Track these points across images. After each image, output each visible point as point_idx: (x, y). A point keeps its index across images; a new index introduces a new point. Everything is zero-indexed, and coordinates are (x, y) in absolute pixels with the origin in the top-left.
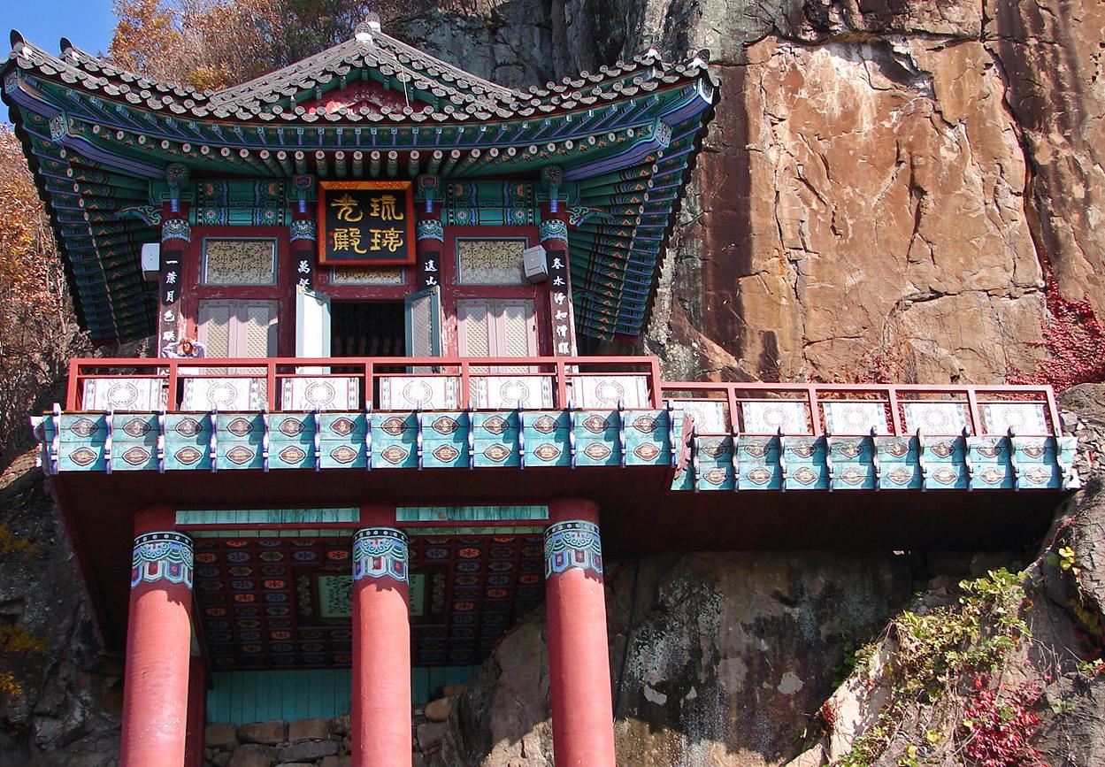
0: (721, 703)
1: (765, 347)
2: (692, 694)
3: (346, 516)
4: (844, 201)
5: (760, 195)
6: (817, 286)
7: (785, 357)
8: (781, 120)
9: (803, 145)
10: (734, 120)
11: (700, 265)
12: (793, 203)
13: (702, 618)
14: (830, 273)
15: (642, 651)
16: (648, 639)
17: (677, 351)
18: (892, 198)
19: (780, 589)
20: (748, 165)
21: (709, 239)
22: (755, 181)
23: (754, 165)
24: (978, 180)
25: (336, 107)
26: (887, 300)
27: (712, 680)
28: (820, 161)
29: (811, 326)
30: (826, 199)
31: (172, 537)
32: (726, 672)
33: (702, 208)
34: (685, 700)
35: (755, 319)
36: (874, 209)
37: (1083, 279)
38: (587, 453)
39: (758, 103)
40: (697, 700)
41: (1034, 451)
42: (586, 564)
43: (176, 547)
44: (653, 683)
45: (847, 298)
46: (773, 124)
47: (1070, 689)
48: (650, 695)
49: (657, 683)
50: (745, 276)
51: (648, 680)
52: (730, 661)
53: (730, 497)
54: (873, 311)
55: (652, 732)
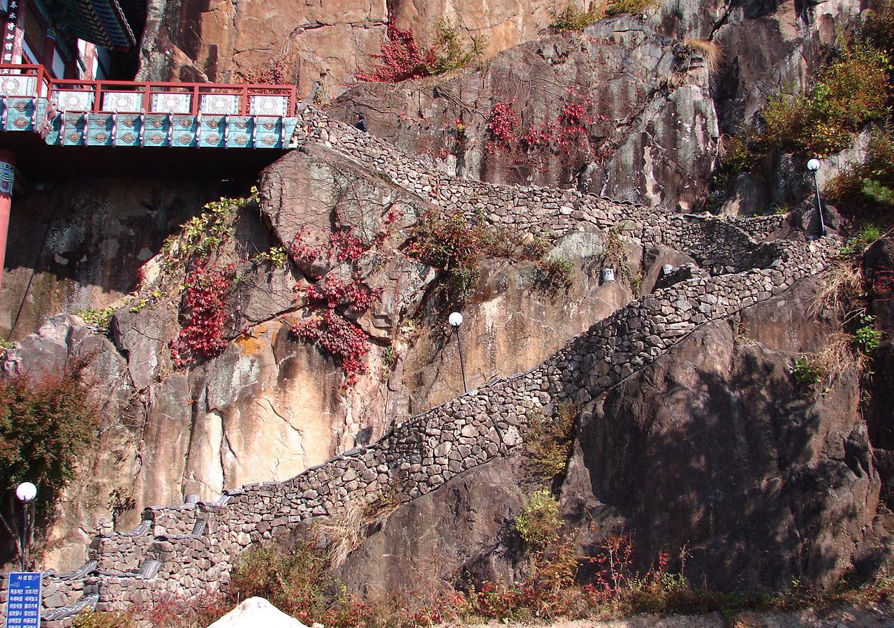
0: (101, 264)
2: (84, 259)
6: (247, 18)
7: (221, 60)
13: (96, 216)
14: (257, 11)
17: (157, 56)
26: (289, 27)
27: (98, 251)
29: (240, 42)
32: (106, 247)
35: (207, 38)
41: (269, 126)
45: (264, 26)
47: (250, 268)
48: (58, 259)
52: (110, 241)
53: (58, 147)
54: (279, 34)
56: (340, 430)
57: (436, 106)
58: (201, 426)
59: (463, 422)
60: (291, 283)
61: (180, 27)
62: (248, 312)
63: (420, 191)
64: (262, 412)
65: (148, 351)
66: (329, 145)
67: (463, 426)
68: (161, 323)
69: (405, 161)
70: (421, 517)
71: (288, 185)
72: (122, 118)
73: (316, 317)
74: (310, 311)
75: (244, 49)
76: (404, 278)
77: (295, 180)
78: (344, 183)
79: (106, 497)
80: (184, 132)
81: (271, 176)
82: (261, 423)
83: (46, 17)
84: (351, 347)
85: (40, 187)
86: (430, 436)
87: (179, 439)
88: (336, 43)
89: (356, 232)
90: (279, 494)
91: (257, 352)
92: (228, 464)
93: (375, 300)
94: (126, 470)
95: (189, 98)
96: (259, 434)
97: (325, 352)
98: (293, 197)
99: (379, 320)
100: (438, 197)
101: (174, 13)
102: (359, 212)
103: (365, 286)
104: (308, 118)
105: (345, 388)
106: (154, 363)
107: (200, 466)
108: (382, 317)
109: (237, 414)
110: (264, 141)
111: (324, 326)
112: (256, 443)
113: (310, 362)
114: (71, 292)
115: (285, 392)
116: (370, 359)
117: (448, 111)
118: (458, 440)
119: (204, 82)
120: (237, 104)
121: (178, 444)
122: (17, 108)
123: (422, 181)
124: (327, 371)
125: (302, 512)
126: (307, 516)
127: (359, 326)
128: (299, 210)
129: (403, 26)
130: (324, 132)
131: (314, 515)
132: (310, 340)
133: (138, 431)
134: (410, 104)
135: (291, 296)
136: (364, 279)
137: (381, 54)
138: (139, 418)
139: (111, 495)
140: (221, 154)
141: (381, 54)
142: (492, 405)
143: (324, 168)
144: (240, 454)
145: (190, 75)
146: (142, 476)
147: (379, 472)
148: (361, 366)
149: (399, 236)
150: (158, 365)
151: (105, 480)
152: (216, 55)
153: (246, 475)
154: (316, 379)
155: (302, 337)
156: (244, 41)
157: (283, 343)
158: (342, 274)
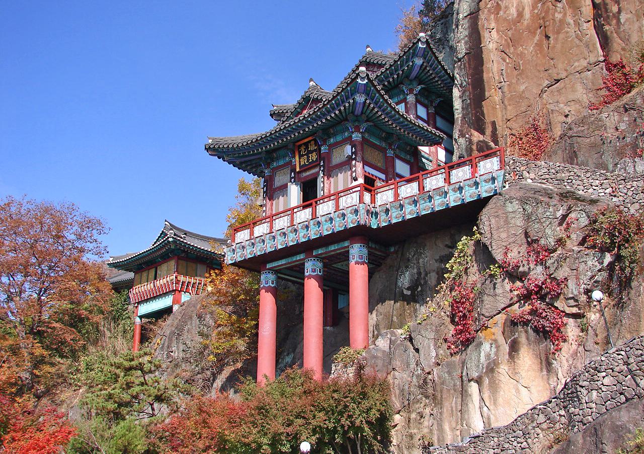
2: (419, 289)
3: (302, 256)
5: (487, 65)
8: (493, 29)
9: (502, 36)
10: (475, 37)
12: (499, 63)
13: (421, 260)
17: (462, 141)
18: (539, 45)
19: (447, 243)
21: (471, 90)
22: (485, 60)
23: (484, 53)
24: (572, 22)
25: (305, 112)
26: (536, 91)
27: (426, 282)
28: (509, 40)
30: (511, 56)
31: (266, 272)
32: (430, 279)
33: (468, 78)
34: (417, 292)
35: (488, 119)
37: (620, 50)
38: (339, 226)
39: (483, 26)
40: (421, 291)
41: (488, 180)
45: (521, 96)
46: (490, 32)
48: (405, 292)
52: (431, 274)
53: (379, 228)
54: (531, 98)
55: (407, 305)
56: (555, 384)
57: (627, 119)
58: (466, 391)
59: (604, 374)
60: (508, 285)
61: (472, 116)
62: (484, 311)
63: (603, 194)
64: (502, 378)
65: (429, 347)
66: (529, 181)
67: (604, 377)
68: (434, 328)
69: (588, 175)
70: (573, 450)
71: (493, 221)
72: (407, 201)
73: (527, 308)
74: (524, 303)
75: (512, 117)
76: (582, 267)
78: (529, 209)
79: (417, 442)
81: (482, 217)
82: (502, 385)
83: (384, 145)
84: (553, 324)
85: (392, 250)
86: (582, 387)
87: (454, 401)
88: (570, 90)
90: (502, 434)
91: (493, 337)
92: (485, 415)
93: (564, 287)
94: (426, 423)
95: (417, 184)
96: (502, 393)
97: (536, 330)
98: (498, 228)
99: (569, 301)
100: (618, 195)
101: (467, 109)
103: (555, 278)
104: (512, 167)
105: (554, 354)
106: (434, 354)
107: (469, 418)
108: (571, 298)
109: (486, 381)
110: (486, 191)
111: (534, 312)
112: (500, 399)
113: (528, 339)
114: (415, 310)
115: (514, 362)
116: (569, 330)
117: (638, 120)
118: (601, 389)
119: (492, 149)
120: (479, 168)
121: (453, 405)
122: (351, 213)
123: (604, 186)
124: (540, 343)
125: (515, 447)
126: (518, 450)
127: (557, 308)
128: (504, 235)
129: (615, 58)
130: (525, 173)
131: (523, 449)
132: (526, 323)
133: (430, 398)
134: (608, 124)
135: (509, 295)
137: (604, 86)
138: (429, 390)
139: (419, 440)
140: (448, 212)
141: (604, 86)
142: (628, 358)
143: (515, 203)
144: (491, 408)
145: (483, 146)
146: (435, 427)
147: (560, 416)
148: (562, 337)
149: (576, 237)
150: (437, 355)
151: (415, 431)
153: (497, 421)
154: (534, 350)
155: (520, 322)
156: (511, 112)
157: (509, 329)
158: (538, 274)
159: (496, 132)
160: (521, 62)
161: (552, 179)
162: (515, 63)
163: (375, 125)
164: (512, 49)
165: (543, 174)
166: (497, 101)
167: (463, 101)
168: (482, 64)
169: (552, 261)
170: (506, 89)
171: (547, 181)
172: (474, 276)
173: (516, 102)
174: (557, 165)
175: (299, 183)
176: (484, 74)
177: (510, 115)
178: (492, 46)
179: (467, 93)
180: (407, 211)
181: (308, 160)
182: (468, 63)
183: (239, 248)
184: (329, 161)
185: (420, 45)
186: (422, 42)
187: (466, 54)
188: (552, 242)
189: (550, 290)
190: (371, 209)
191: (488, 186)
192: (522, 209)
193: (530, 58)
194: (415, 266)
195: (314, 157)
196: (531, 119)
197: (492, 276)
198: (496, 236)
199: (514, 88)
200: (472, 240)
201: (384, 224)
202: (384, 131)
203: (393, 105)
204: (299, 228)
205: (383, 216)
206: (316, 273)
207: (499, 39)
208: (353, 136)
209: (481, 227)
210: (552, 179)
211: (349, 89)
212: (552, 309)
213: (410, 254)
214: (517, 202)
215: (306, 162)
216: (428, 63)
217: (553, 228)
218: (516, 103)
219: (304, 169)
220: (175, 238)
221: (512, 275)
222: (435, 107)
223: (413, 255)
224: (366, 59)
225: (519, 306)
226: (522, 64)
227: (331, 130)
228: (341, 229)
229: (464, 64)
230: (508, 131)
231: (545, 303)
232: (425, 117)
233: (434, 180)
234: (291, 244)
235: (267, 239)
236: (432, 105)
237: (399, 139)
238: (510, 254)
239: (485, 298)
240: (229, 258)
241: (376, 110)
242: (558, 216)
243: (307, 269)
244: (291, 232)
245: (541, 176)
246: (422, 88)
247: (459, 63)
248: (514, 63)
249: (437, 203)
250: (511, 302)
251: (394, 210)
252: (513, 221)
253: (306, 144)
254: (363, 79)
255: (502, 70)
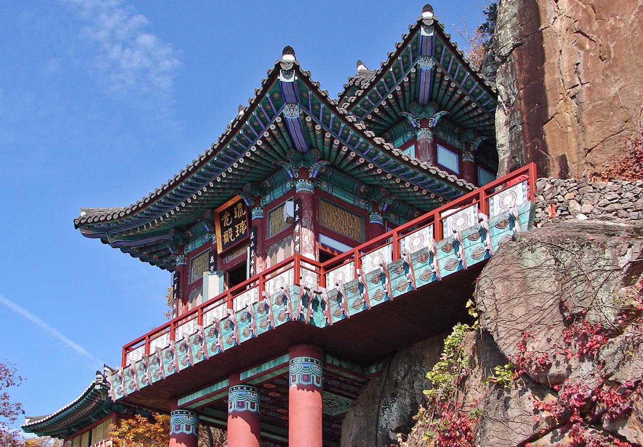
1: (561, 167)
3: (225, 384)
4: (608, 31)
5: (551, 60)
9: (577, 5)
11: (521, 129)
12: (571, 53)
15: (385, 412)
16: (388, 404)
20: (541, 43)
21: (523, 108)
22: (547, 51)
23: (545, 40)
30: (595, 37)
31: (176, 413)
35: (554, 153)
36: (631, 25)
38: (261, 327)
41: (502, 224)
42: (297, 382)
43: (178, 417)
44: (393, 429)
45: (612, 105)
49: (395, 429)
50: (546, 123)
51: (390, 428)
53: (328, 327)
54: (631, 106)
60: (529, 401)
61: (526, 152)
66: (581, 217)
71: (499, 287)
74: (563, 433)
75: (595, 144)
77: (507, 278)
80: (423, 269)
83: (362, 204)
85: (374, 371)
89: (592, 317)
98: (509, 300)
101: (517, 141)
102: (590, 289)
103: (617, 383)
104: (549, 196)
127: (623, 439)
128: (519, 311)
135: (532, 420)
136: (612, 374)
143: (539, 250)
152: (566, 164)
156: (594, 133)
158: (583, 377)
159: (567, 173)
160: (612, 45)
161: (625, 209)
162: (601, 49)
163: (333, 166)
164: (596, 25)
165: (608, 202)
166: (569, 120)
167: (511, 129)
168: (543, 60)
169: (611, 350)
170: (583, 97)
171: (616, 215)
172: (477, 391)
173: (603, 117)
174: (637, 185)
175: (222, 272)
176: (546, 76)
177: (592, 141)
178: (559, 25)
179: (518, 115)
180: (371, 294)
181: (234, 233)
182: (519, 63)
183: (128, 375)
184: (264, 233)
185: (423, 32)
186: (427, 28)
187: (515, 46)
188: (610, 315)
189: (607, 405)
190: (311, 294)
191: (503, 234)
192: (553, 261)
193: (628, 34)
194: (407, 394)
195: (242, 228)
196: (629, 143)
197: (500, 386)
198: (505, 313)
199: (599, 93)
200: (473, 330)
201: (336, 320)
202: (363, 183)
203: (396, 152)
204: (206, 334)
205: (334, 307)
206: (245, 409)
207: (572, 11)
208: (297, 186)
209: (479, 300)
210: (625, 209)
211: (268, 95)
212: (616, 441)
213: (399, 374)
214: (543, 248)
215: (231, 237)
216: (460, 82)
217: (612, 289)
218: (601, 119)
219: (230, 249)
220: (105, 385)
221: (539, 384)
222: (474, 153)
223: (402, 375)
224: (354, 83)
225: (552, 438)
226: (613, 47)
227: (267, 182)
228: (264, 331)
229: (512, 65)
230: (588, 170)
231: (602, 431)
232: (454, 167)
233: (417, 239)
234: (196, 361)
235: (164, 356)
236: (468, 149)
237: (391, 194)
238: (532, 345)
239: (489, 425)
240: (116, 391)
241: (345, 149)
242: (622, 266)
243: (231, 403)
244: (195, 342)
245: (604, 206)
246: (443, 117)
247: (504, 66)
248: (598, 49)
249: (417, 274)
250: (536, 432)
251: (350, 294)
252: (536, 285)
253: (231, 210)
254: (288, 73)
255: (577, 64)
